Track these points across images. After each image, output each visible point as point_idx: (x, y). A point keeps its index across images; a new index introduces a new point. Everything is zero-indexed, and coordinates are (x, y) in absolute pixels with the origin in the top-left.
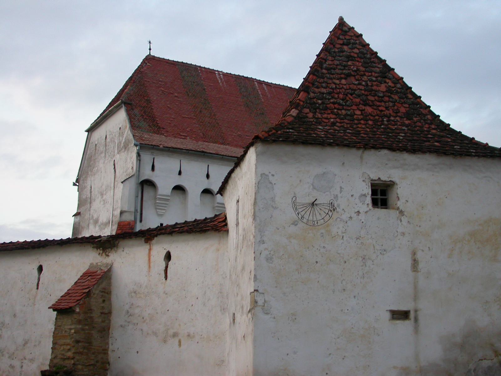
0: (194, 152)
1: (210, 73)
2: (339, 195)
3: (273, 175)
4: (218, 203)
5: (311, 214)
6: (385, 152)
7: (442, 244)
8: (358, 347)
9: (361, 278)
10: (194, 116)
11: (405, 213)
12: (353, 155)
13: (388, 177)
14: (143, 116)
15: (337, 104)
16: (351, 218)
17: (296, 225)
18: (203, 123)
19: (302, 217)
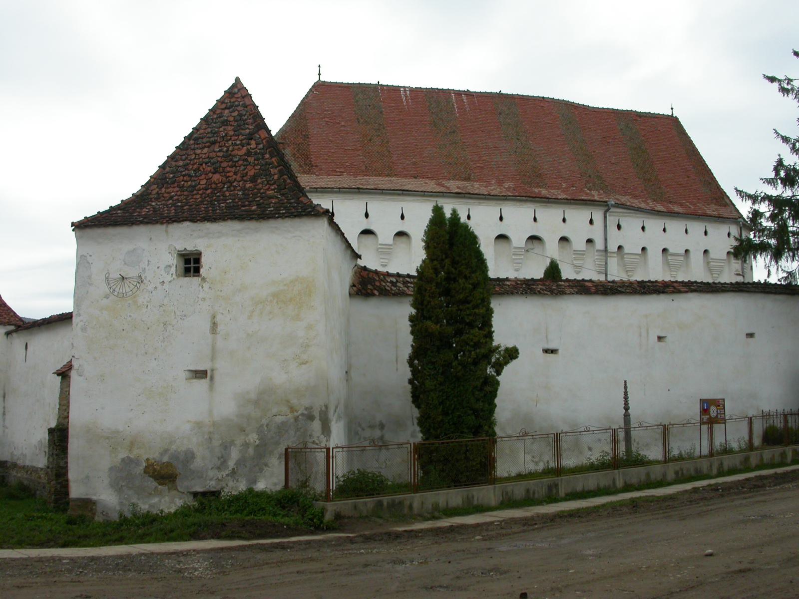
0: (347, 190)
1: (394, 90)
2: (147, 268)
3: (90, 256)
4: (380, 244)
5: (122, 287)
7: (242, 306)
8: (156, 403)
9: (161, 342)
10: (360, 146)
11: (207, 280)
12: (158, 230)
15: (187, 176)
16: (156, 288)
17: (108, 298)
18: (369, 153)
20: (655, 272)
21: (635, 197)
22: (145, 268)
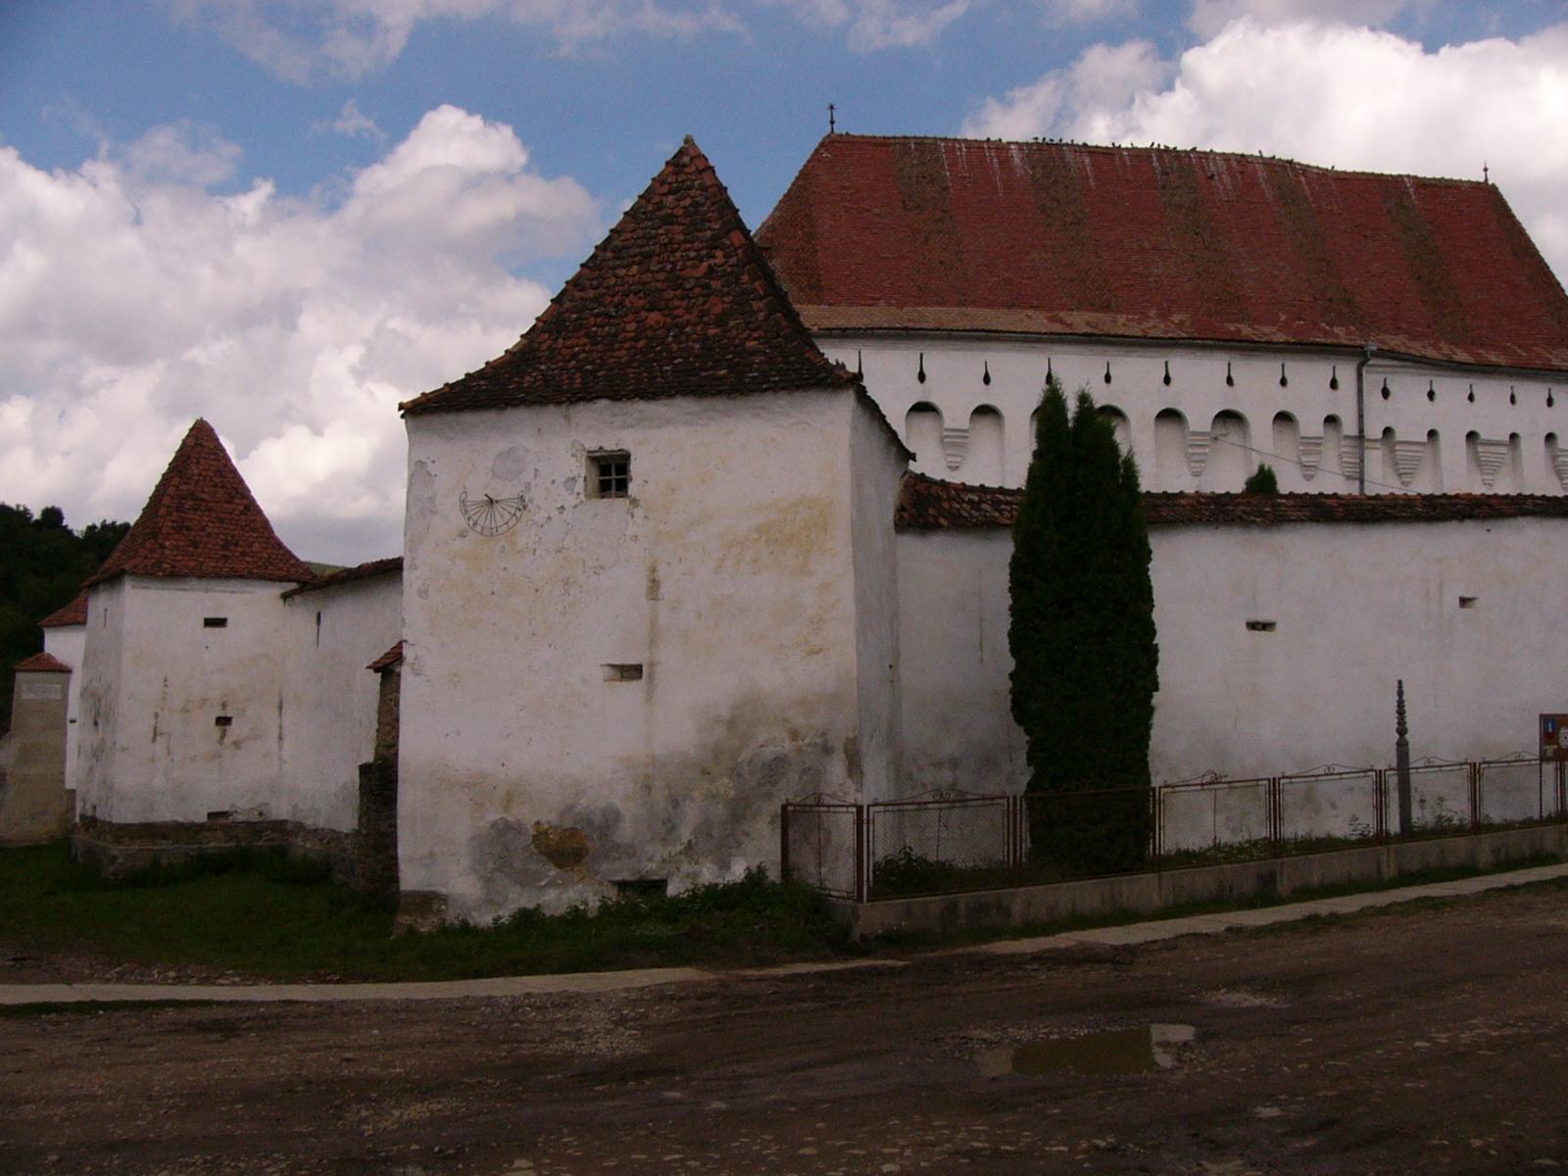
2: (533, 482)
3: (433, 462)
6: (603, 403)
12: (551, 416)
13: (617, 445)
14: (791, 269)
16: (549, 518)
17: (465, 537)
19: (475, 523)
20: (1456, 477)
21: (1415, 337)
22: (529, 483)
